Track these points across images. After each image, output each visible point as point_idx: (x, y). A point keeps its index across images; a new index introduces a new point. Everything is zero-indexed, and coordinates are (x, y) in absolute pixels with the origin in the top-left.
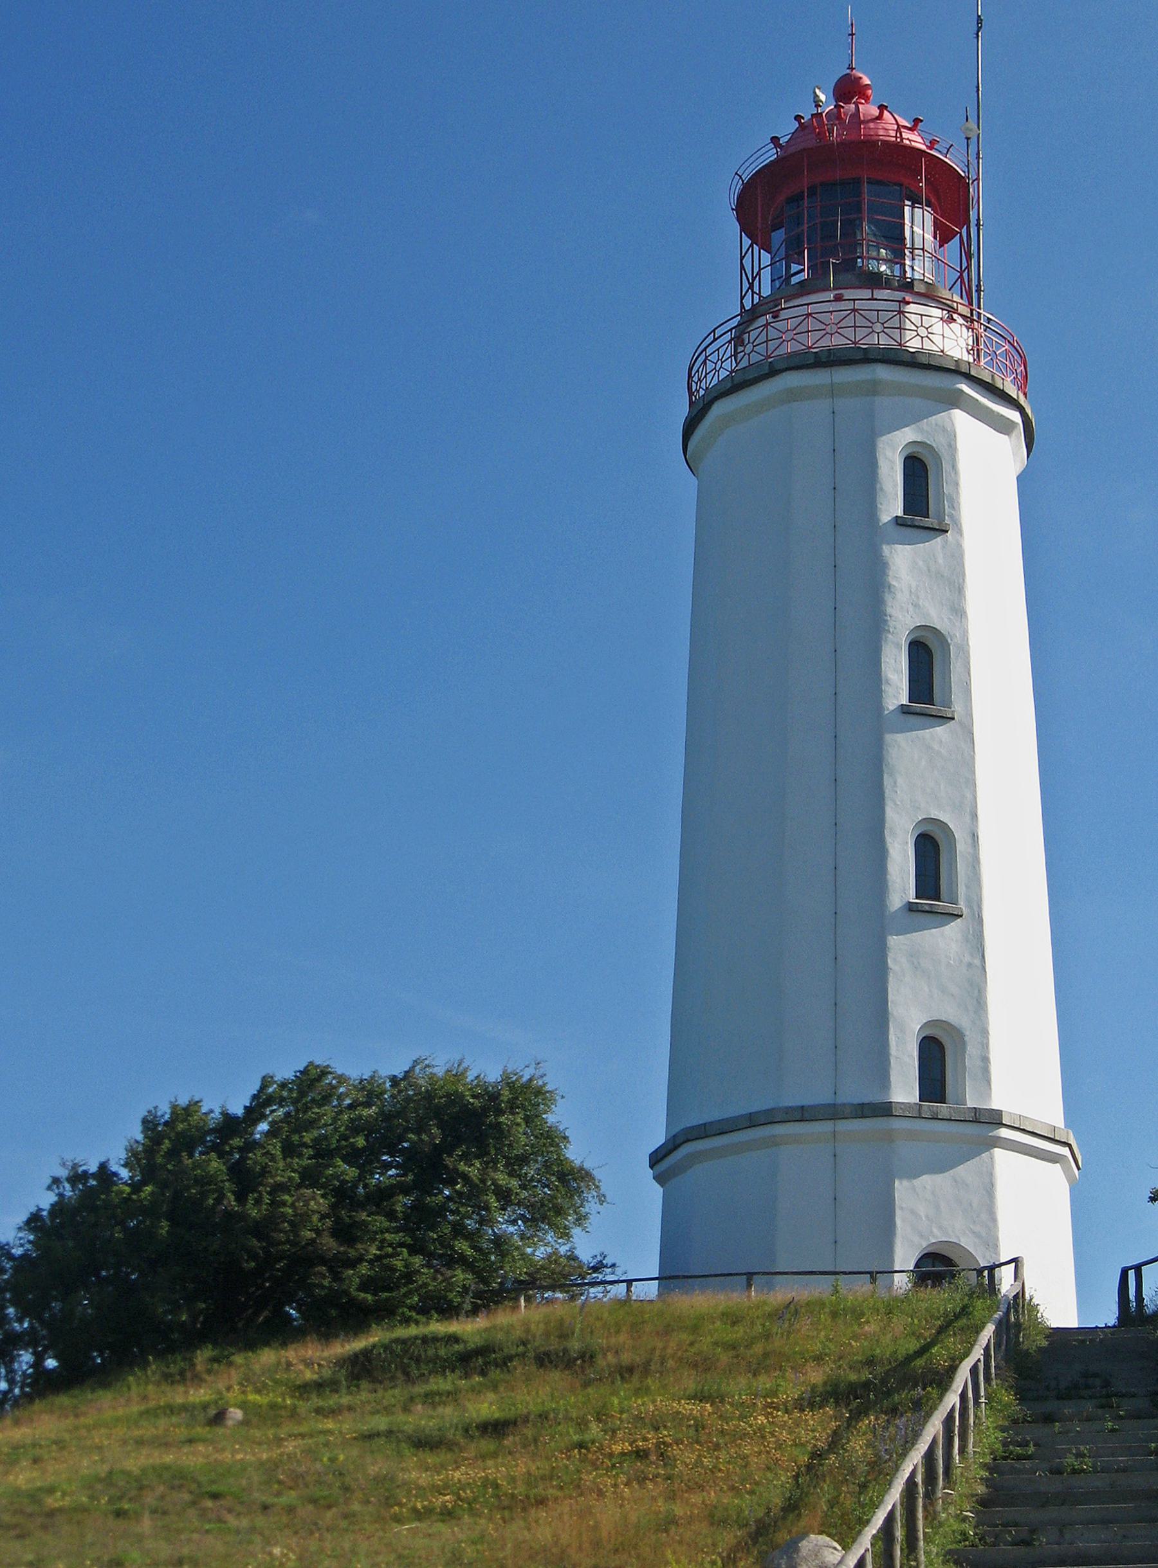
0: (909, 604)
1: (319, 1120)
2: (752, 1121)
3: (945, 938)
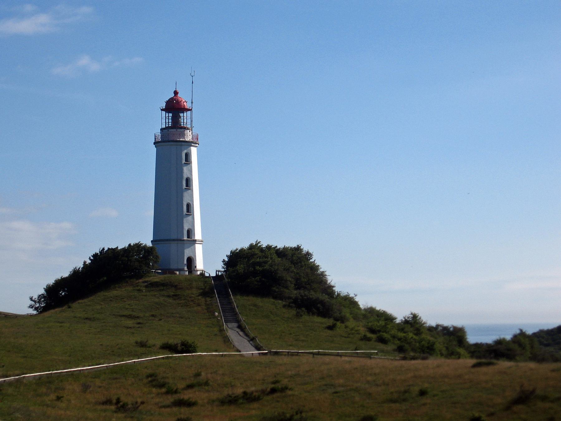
0: (186, 174)
1: (290, 303)
2: (167, 240)
3: (190, 218)
